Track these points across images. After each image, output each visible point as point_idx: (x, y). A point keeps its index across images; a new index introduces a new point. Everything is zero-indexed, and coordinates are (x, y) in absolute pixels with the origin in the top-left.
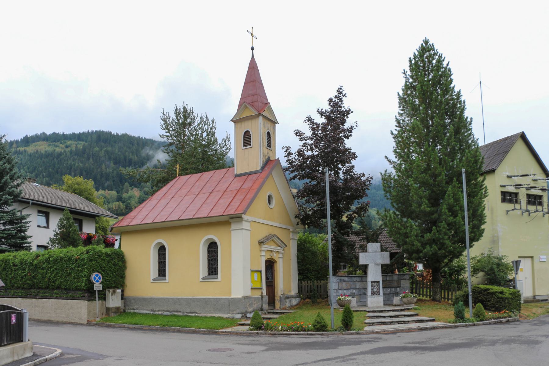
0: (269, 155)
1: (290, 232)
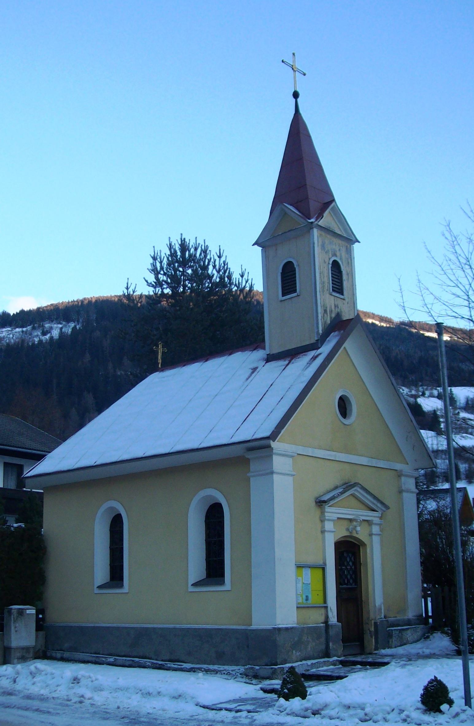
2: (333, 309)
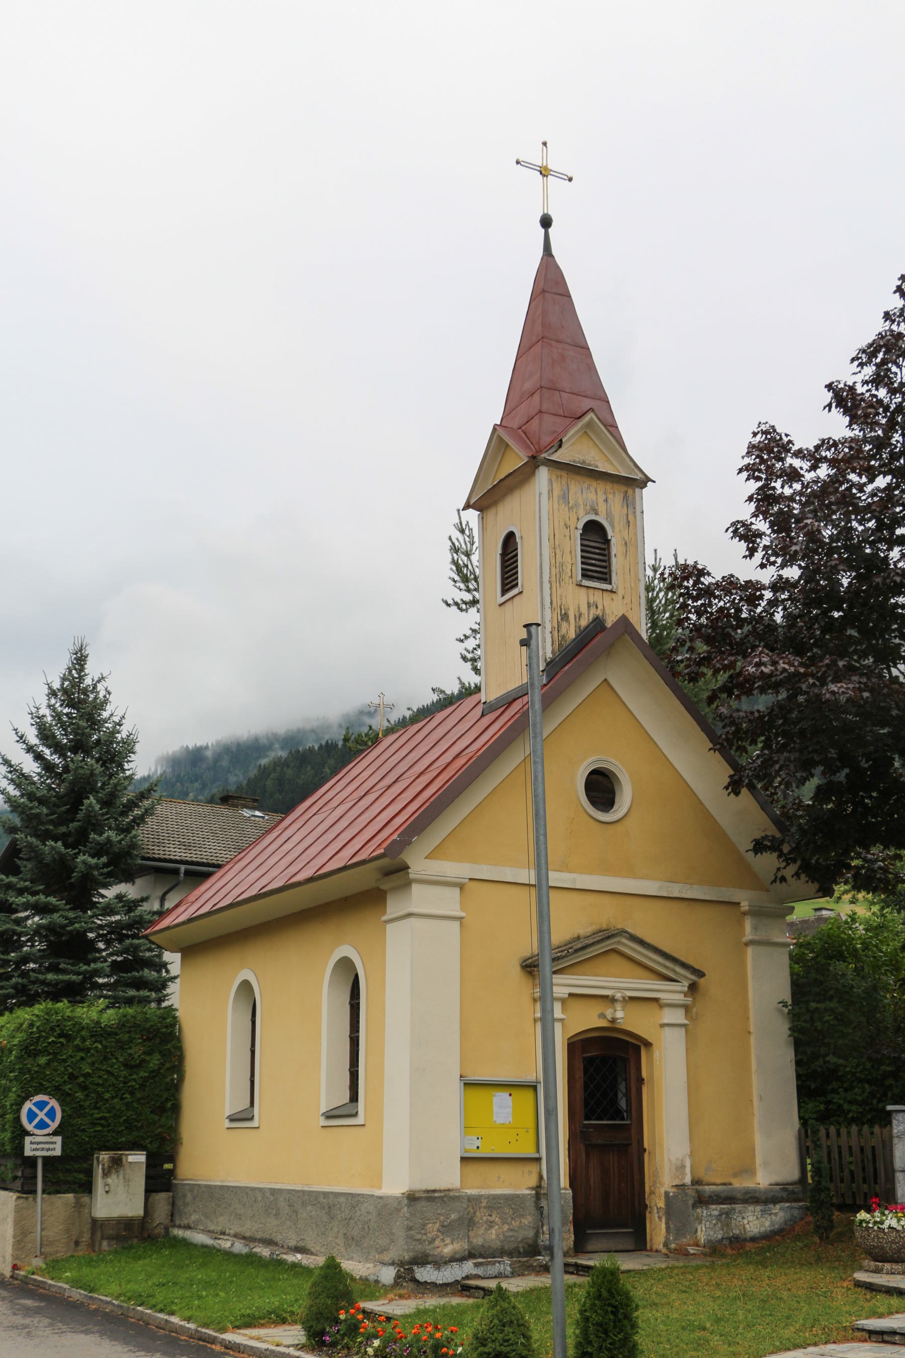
0: (593, 613)
1: (745, 914)
2: (584, 609)
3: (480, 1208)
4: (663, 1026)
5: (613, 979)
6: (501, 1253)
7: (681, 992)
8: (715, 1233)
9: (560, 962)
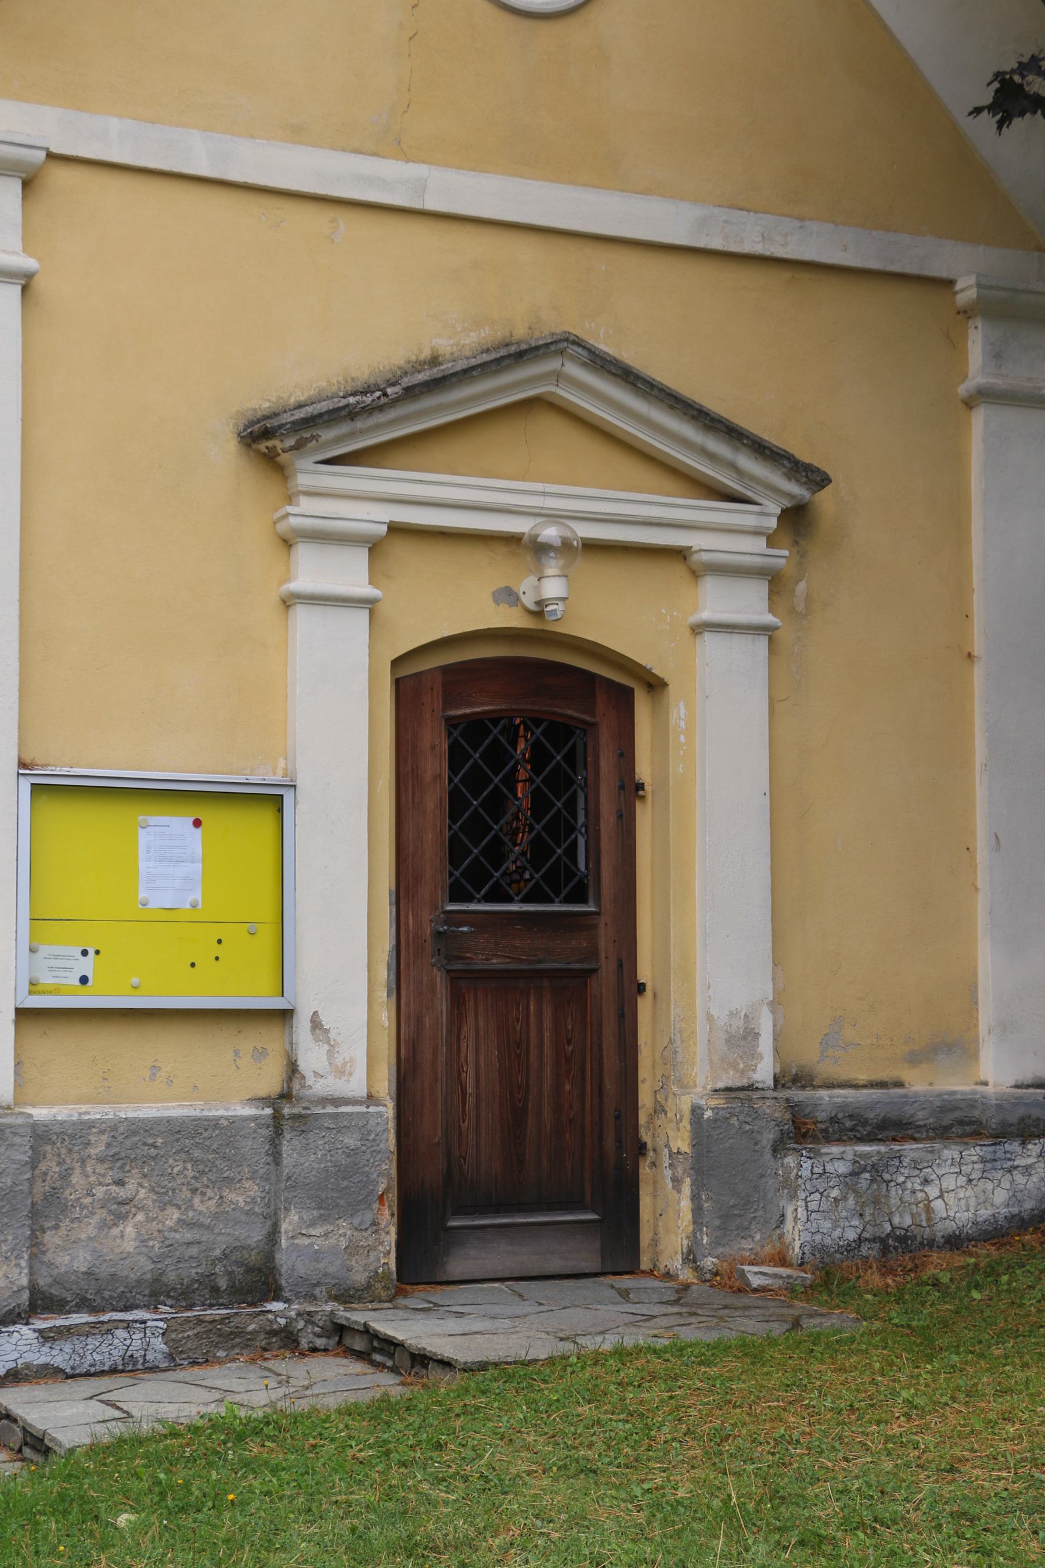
1: (966, 313)
3: (83, 1161)
4: (699, 629)
5: (539, 487)
6: (154, 1294)
7: (756, 533)
8: (835, 1227)
9: (359, 424)
